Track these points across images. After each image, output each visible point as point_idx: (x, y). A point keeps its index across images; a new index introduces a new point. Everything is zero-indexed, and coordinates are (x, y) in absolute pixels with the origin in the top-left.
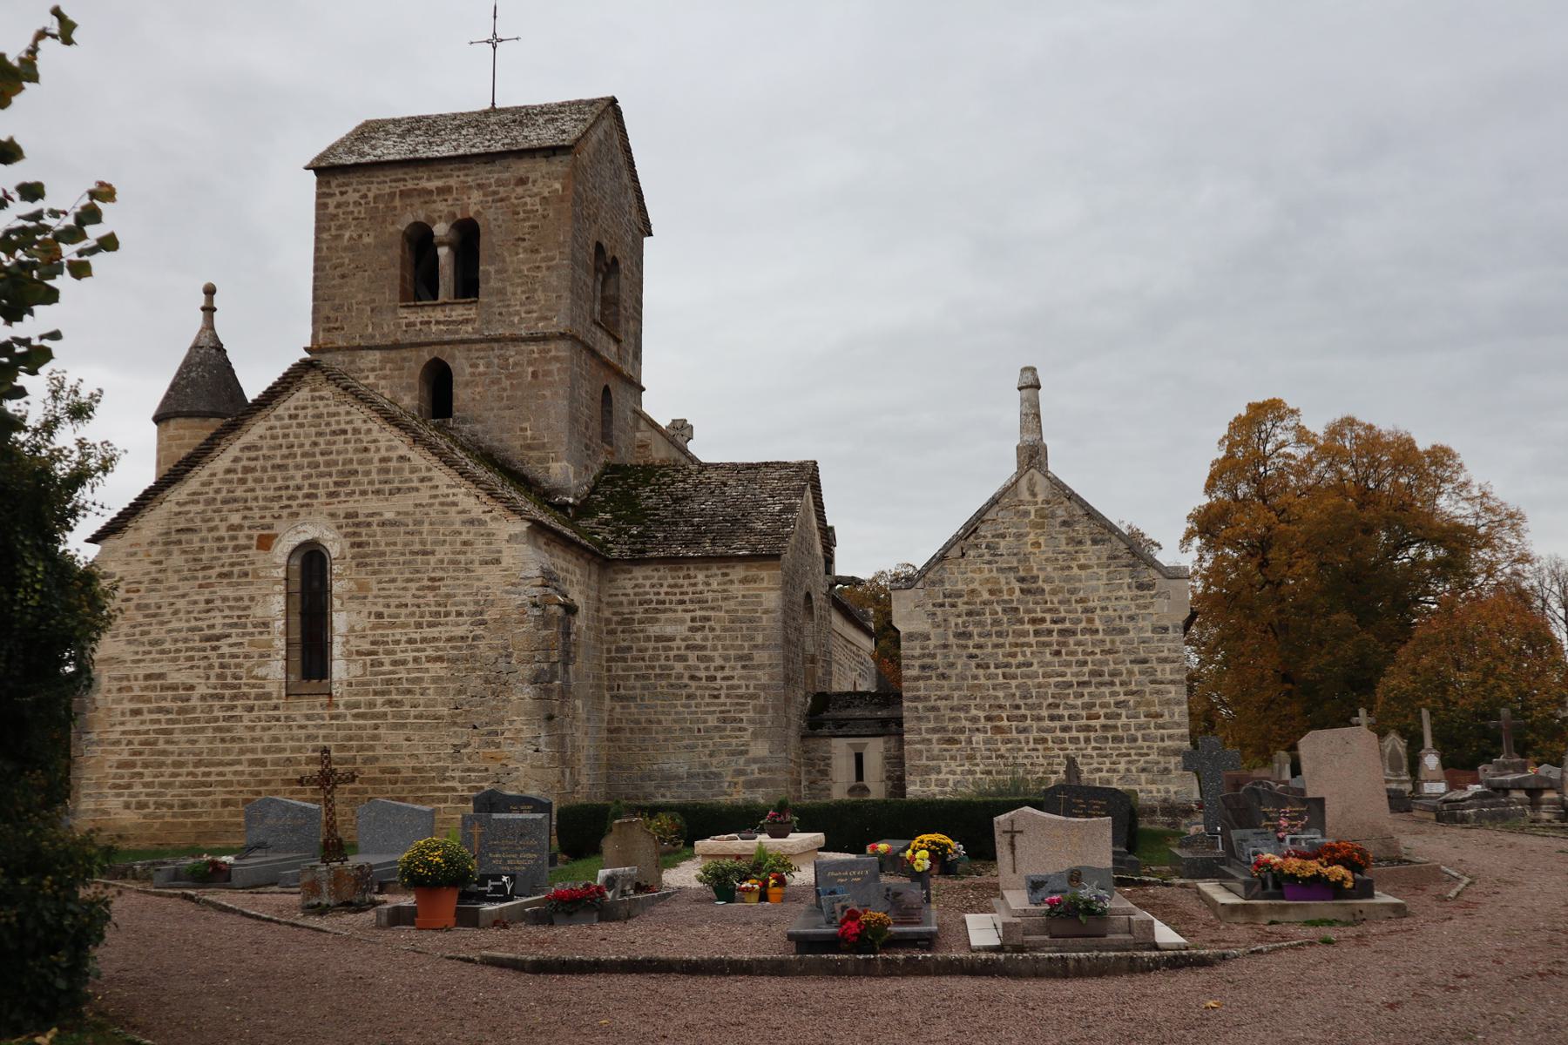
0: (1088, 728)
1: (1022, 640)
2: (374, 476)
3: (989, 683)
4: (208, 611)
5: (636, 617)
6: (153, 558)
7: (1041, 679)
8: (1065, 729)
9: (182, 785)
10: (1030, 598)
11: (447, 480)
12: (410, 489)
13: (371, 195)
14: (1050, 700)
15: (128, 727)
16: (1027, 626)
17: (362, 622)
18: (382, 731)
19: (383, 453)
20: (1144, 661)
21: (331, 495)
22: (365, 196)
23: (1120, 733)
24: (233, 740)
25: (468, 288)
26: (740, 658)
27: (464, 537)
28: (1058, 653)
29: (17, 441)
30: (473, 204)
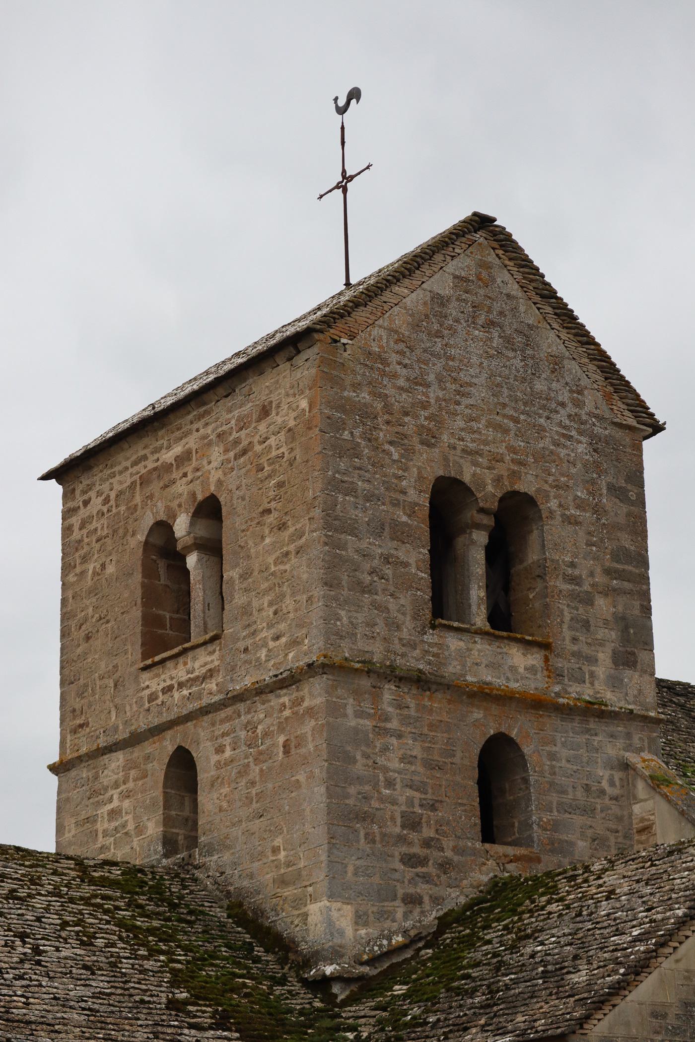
29: (360, 919)
30: (214, 471)
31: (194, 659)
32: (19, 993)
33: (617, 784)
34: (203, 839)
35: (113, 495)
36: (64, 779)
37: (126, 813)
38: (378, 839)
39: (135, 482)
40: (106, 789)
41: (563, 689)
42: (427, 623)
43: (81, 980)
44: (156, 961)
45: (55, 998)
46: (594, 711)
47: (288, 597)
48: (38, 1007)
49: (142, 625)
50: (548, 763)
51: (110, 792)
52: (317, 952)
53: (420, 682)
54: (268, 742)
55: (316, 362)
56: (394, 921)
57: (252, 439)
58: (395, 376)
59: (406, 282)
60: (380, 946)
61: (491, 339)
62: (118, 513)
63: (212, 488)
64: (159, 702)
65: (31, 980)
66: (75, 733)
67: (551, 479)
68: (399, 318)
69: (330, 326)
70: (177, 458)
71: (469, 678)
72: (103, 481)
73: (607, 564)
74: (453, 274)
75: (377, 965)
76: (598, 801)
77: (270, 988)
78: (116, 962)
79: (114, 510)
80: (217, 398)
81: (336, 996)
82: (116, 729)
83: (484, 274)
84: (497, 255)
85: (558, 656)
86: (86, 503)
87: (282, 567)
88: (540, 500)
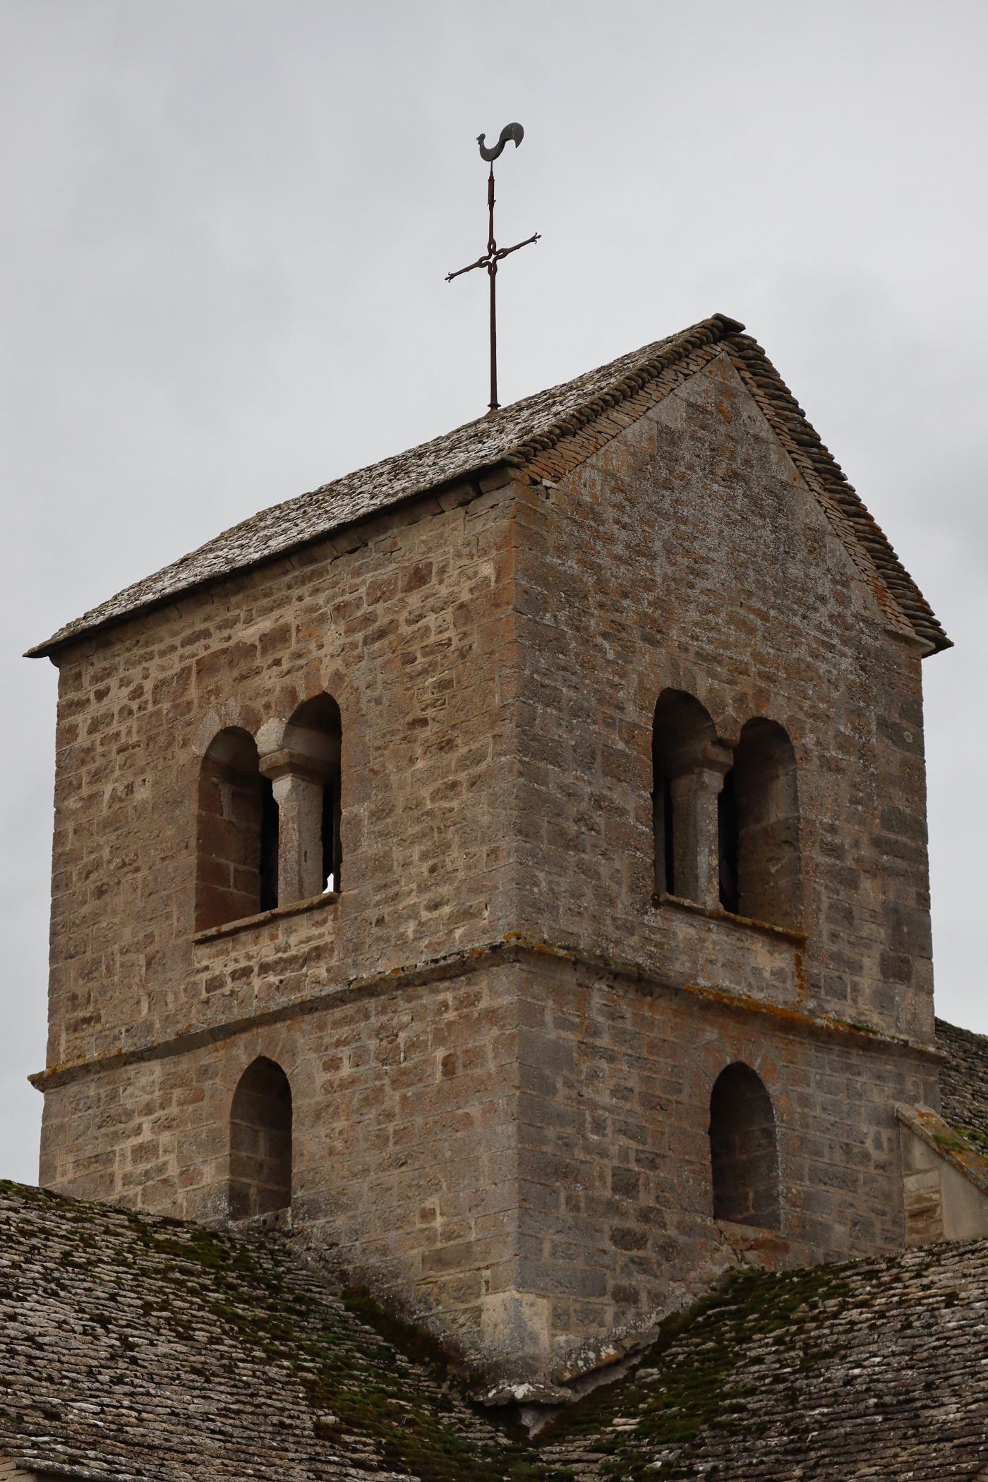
29: (559, 1320)
30: (328, 658)
31: (289, 931)
32: (126, 1403)
33: (885, 1145)
34: (299, 1194)
35: (148, 686)
36: (54, 1097)
37: (165, 1151)
38: (583, 1205)
39: (189, 669)
40: (130, 1115)
41: (819, 1005)
42: (649, 897)
43: (194, 1389)
44: (278, 1366)
45: (173, 1414)
46: (858, 1040)
47: (455, 847)
48: (156, 1425)
49: (198, 878)
50: (799, 1110)
51: (137, 1120)
52: (497, 1365)
53: (642, 983)
54: (417, 1057)
55: (508, 511)
56: (602, 1325)
57: (395, 617)
58: (610, 539)
59: (627, 405)
60: (586, 1360)
61: (733, 498)
62: (157, 713)
63: (325, 684)
64: (226, 990)
65: (132, 1384)
66: (75, 1030)
67: (807, 704)
68: (616, 457)
69: (528, 460)
70: (263, 638)
71: (702, 982)
72: (130, 664)
73: (877, 831)
74: (686, 401)
75: (579, 1388)
76: (861, 1168)
77: (434, 1413)
78: (230, 1366)
79: (150, 708)
80: (335, 554)
81: (527, 1429)
82: (149, 1027)
83: (726, 405)
84: (743, 379)
85: (812, 957)
86: (101, 695)
87: (446, 805)
88: (792, 732)
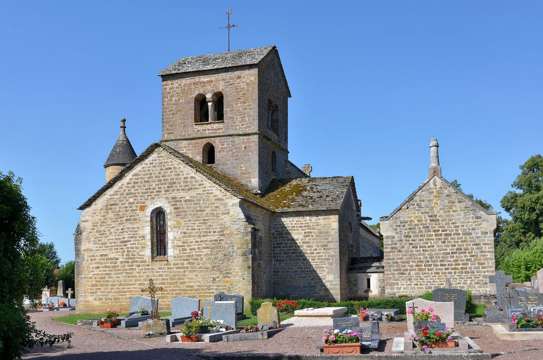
0: (455, 269)
1: (431, 238)
2: (182, 184)
3: (417, 253)
4: (123, 232)
5: (284, 232)
6: (102, 215)
7: (437, 252)
8: (446, 269)
9: (115, 292)
10: (433, 223)
11: (209, 185)
12: (195, 188)
13: (182, 84)
14: (441, 259)
15: (95, 273)
16: (432, 233)
17: (178, 235)
18: (186, 273)
19: (185, 176)
20: (478, 245)
21: (166, 191)
22: (180, 85)
23: (468, 270)
24: (133, 276)
25: (220, 117)
26: (323, 246)
27: (216, 205)
28: (444, 242)
30: (221, 87)
